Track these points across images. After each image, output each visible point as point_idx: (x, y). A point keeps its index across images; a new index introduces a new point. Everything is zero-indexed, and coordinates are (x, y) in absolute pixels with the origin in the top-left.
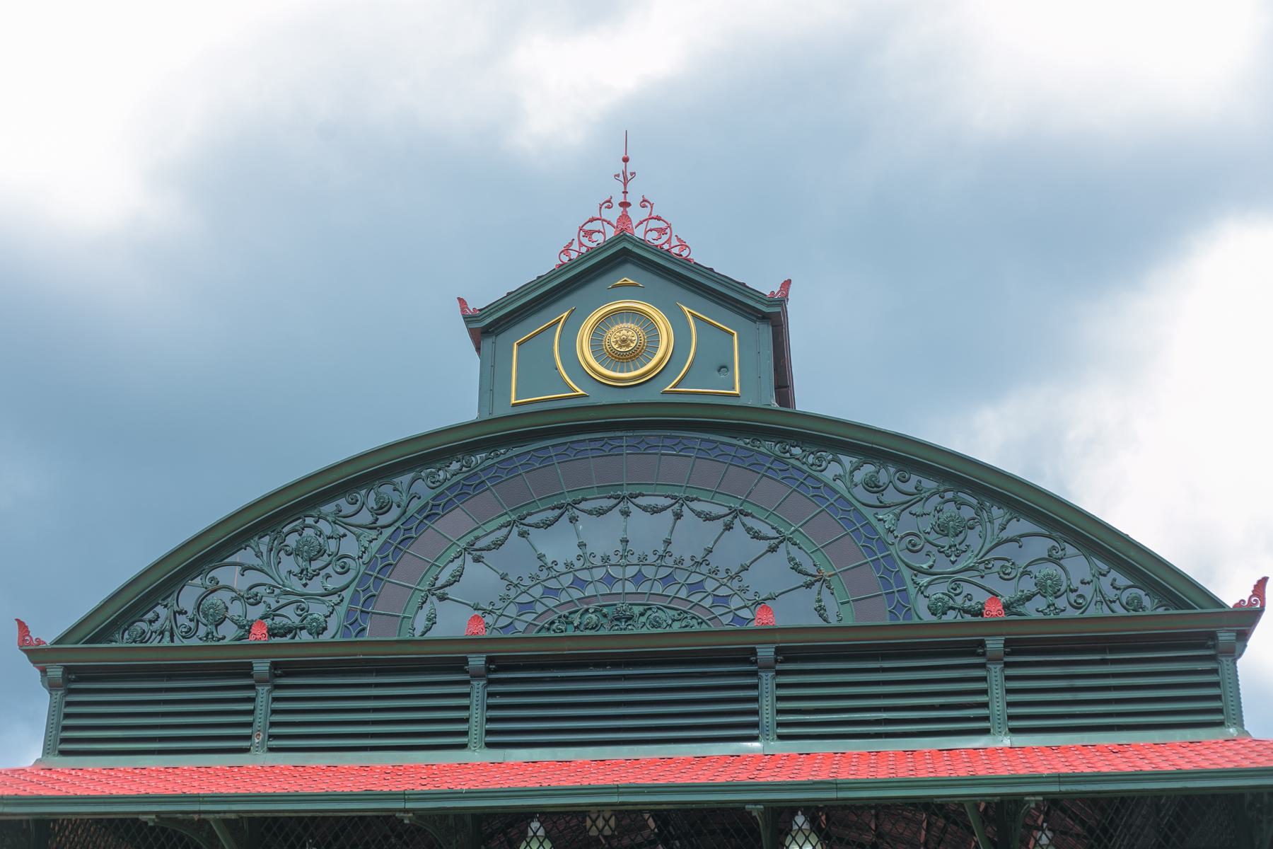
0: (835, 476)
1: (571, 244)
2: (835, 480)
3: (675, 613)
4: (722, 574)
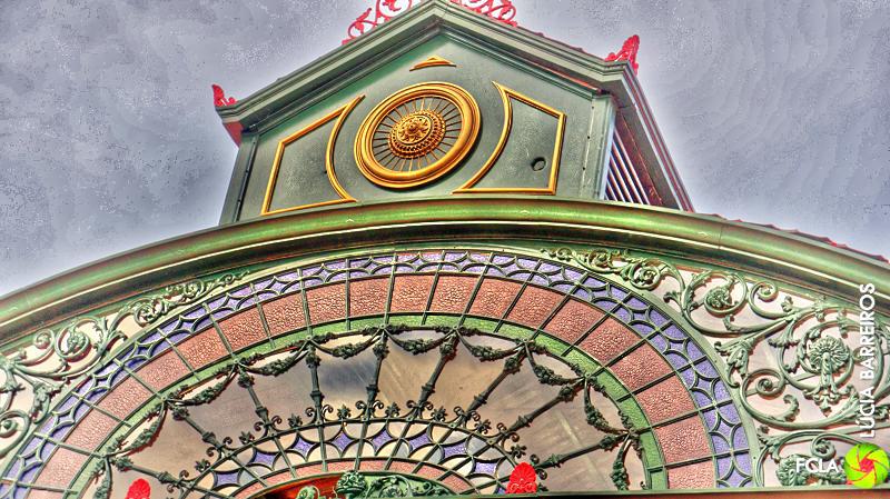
0: (668, 294)
1: (366, 14)
2: (667, 300)
3: (420, 485)
4: (451, 416)
